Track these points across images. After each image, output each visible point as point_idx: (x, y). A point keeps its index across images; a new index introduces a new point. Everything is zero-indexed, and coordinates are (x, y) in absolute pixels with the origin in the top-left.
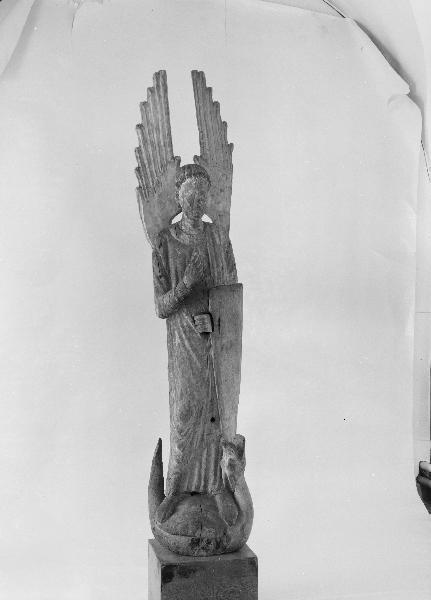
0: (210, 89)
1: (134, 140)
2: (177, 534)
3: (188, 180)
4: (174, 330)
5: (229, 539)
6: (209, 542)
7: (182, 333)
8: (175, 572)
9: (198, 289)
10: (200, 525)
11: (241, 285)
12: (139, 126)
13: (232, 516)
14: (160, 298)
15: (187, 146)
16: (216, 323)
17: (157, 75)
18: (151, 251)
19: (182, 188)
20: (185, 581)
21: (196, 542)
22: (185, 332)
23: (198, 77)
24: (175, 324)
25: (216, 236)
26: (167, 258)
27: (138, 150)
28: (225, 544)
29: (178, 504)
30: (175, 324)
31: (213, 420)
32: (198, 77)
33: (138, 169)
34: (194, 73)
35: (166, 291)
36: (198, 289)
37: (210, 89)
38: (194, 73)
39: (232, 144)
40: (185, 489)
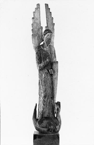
0: (49, 9)
1: (31, 22)
2: (44, 128)
3: (48, 34)
4: (42, 74)
5: (56, 129)
6: (52, 130)
7: (45, 74)
8: (37, 136)
9: (47, 62)
10: (50, 125)
11: (57, 62)
12: (33, 18)
13: (57, 123)
14: (40, 65)
15: (44, 24)
16: (54, 72)
17: (38, 4)
18: (35, 53)
19: (46, 36)
20: (40, 139)
21: (49, 130)
22: (46, 74)
23: (47, 5)
24: (43, 72)
25: (52, 48)
26: (40, 54)
27: (32, 25)
28: (55, 130)
29: (43, 120)
30: (43, 72)
31: (52, 98)
32: (47, 5)
33: (32, 30)
34: (46, 4)
35: (41, 63)
36: (47, 62)
37: (49, 9)
38: (46, 4)
39: (54, 23)
40: (44, 116)
